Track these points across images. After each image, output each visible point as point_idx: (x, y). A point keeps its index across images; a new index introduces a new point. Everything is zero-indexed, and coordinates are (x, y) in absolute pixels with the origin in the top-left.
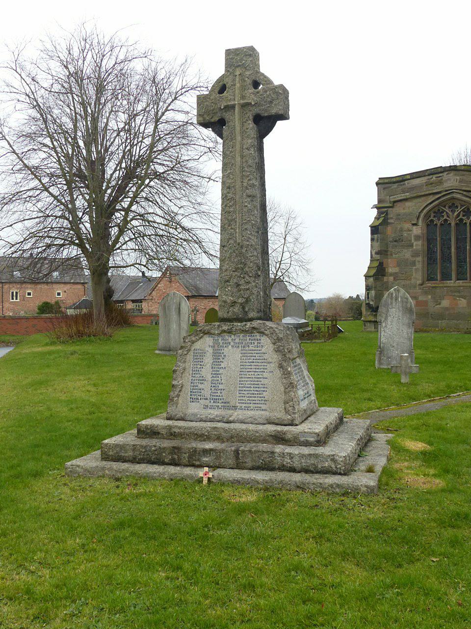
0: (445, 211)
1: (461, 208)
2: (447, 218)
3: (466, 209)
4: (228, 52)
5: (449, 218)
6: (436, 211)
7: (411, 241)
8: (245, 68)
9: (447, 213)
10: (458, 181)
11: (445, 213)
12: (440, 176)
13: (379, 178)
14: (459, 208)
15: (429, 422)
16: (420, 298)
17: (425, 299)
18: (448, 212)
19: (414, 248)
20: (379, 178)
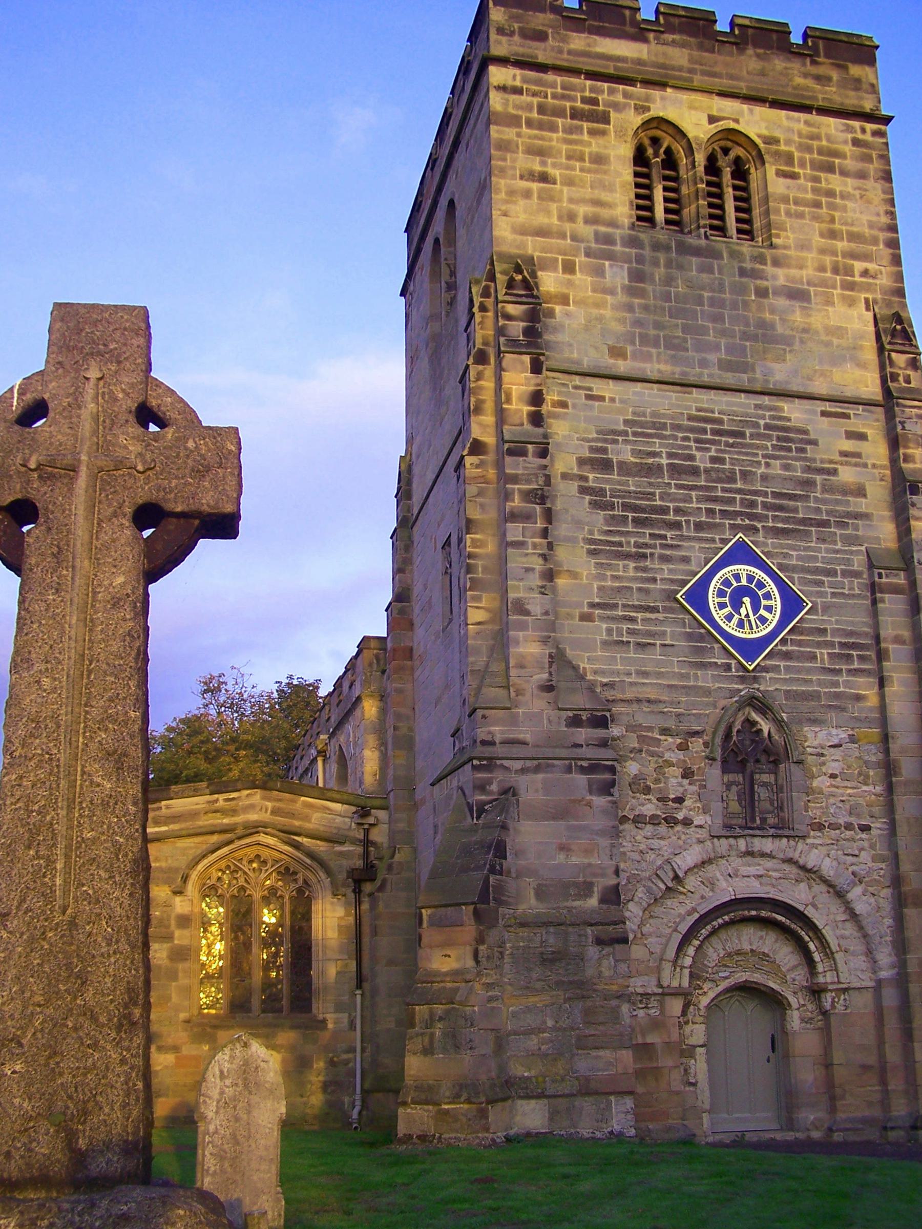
0: (241, 869)
1: (272, 866)
2: (245, 885)
3: (282, 870)
4: (57, 306)
5: (249, 883)
6: (223, 867)
7: (168, 927)
8: (119, 362)
9: (245, 873)
10: (269, 811)
11: (240, 873)
12: (233, 799)
13: (401, 295)
14: (269, 865)
15: (259, 777)
16: (186, 1050)
17: (194, 1053)
18: (247, 871)
19: (176, 942)
20: (401, 295)
